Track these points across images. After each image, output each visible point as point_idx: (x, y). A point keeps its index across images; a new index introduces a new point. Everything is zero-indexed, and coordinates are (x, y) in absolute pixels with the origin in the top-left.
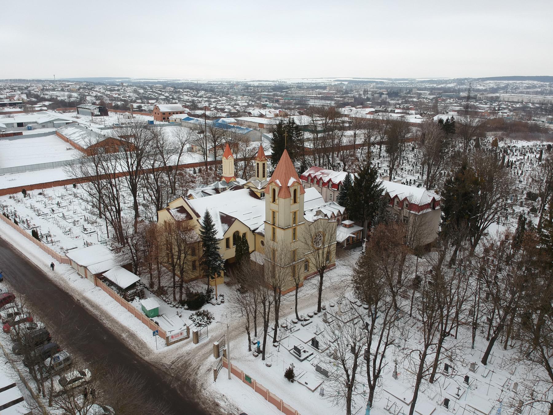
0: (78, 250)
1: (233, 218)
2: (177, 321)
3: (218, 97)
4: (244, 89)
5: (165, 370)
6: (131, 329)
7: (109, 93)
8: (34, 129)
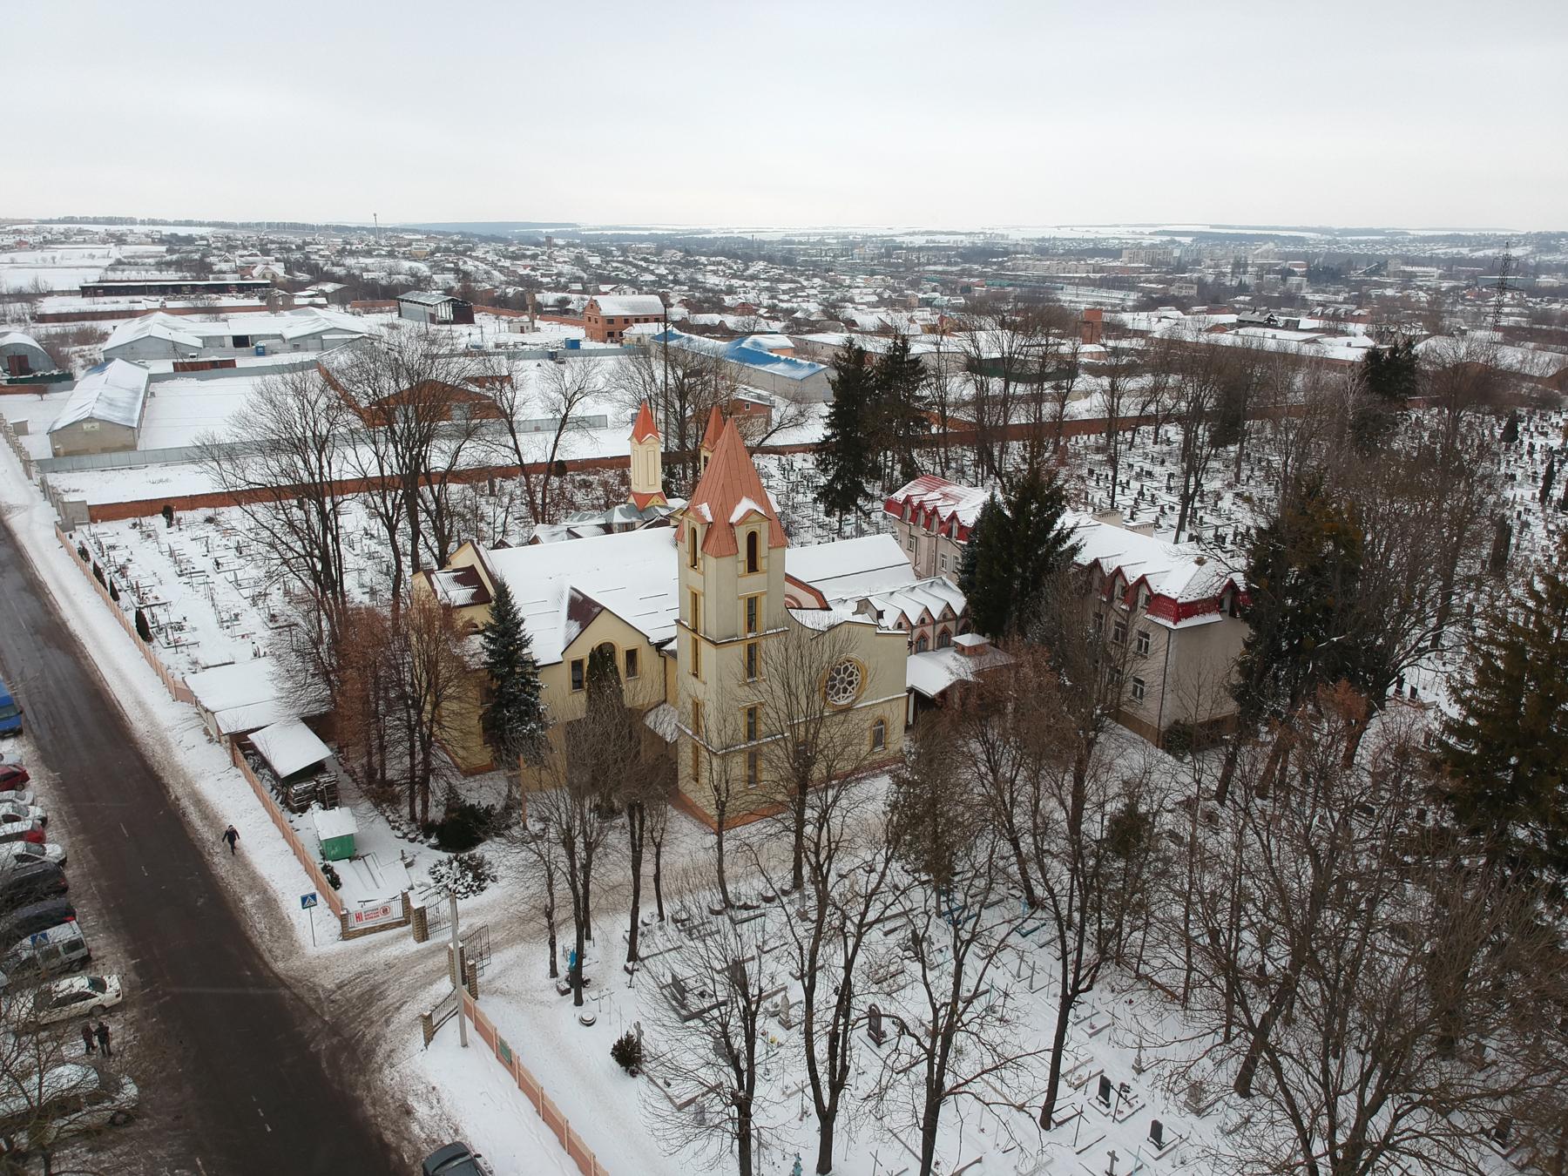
0: (208, 670)
1: (596, 604)
2: (394, 872)
3: (801, 279)
4: (881, 256)
5: (312, 1002)
6: (273, 884)
7: (507, 263)
8: (273, 353)
